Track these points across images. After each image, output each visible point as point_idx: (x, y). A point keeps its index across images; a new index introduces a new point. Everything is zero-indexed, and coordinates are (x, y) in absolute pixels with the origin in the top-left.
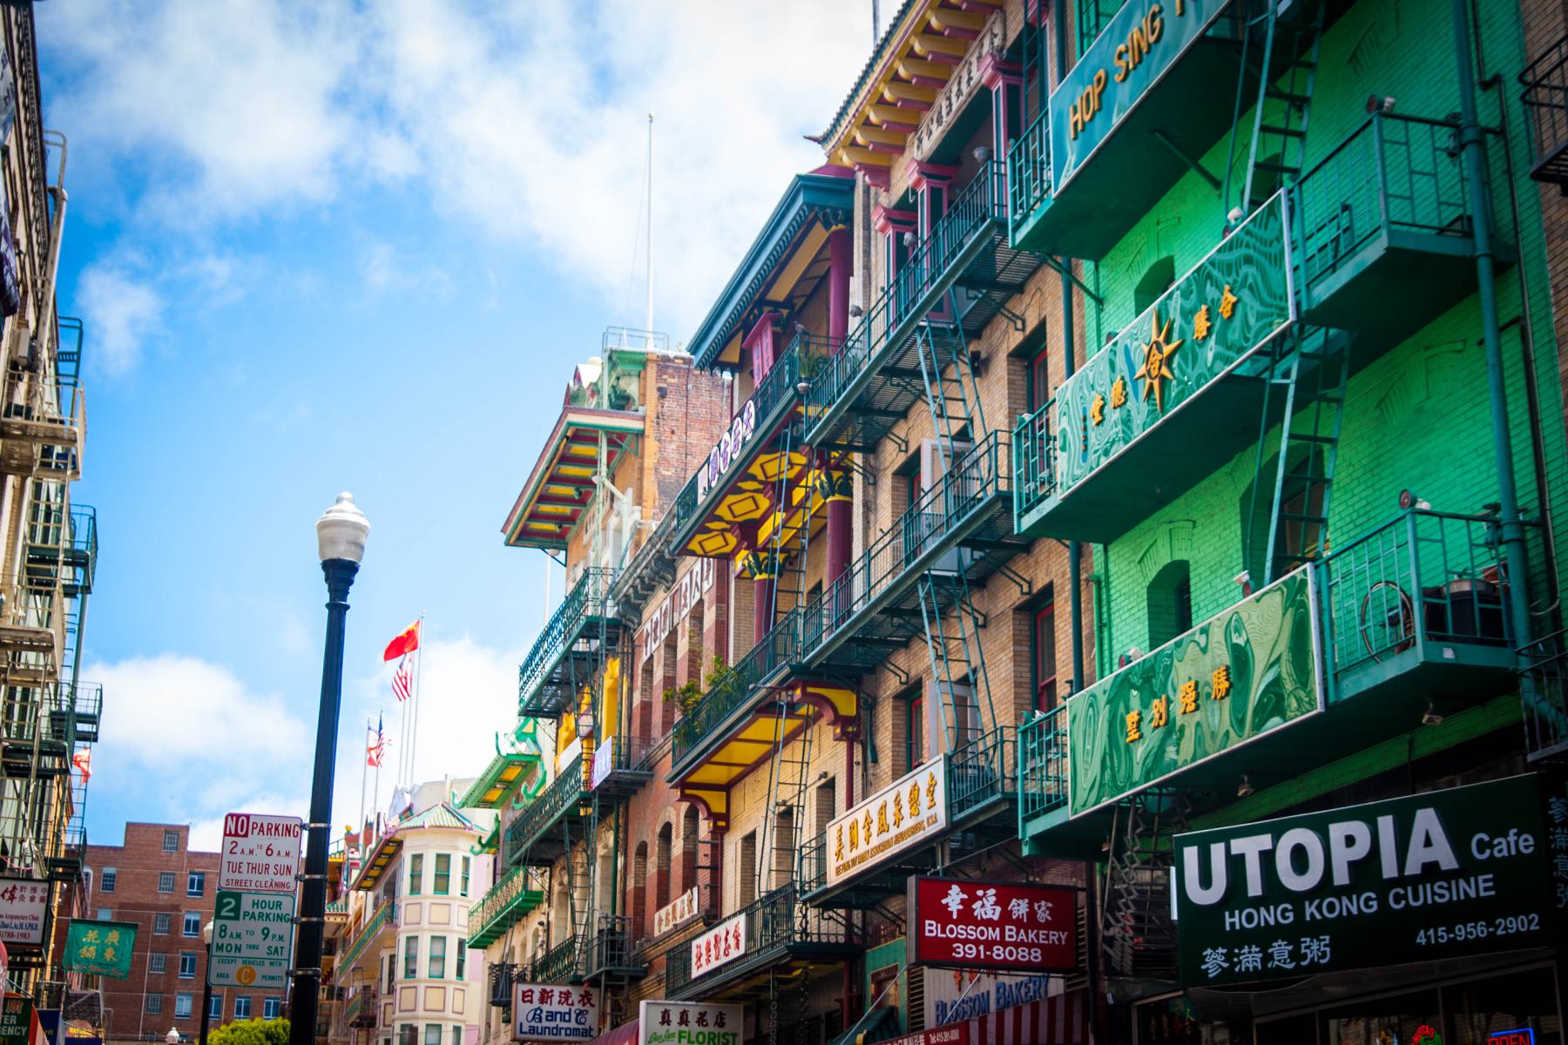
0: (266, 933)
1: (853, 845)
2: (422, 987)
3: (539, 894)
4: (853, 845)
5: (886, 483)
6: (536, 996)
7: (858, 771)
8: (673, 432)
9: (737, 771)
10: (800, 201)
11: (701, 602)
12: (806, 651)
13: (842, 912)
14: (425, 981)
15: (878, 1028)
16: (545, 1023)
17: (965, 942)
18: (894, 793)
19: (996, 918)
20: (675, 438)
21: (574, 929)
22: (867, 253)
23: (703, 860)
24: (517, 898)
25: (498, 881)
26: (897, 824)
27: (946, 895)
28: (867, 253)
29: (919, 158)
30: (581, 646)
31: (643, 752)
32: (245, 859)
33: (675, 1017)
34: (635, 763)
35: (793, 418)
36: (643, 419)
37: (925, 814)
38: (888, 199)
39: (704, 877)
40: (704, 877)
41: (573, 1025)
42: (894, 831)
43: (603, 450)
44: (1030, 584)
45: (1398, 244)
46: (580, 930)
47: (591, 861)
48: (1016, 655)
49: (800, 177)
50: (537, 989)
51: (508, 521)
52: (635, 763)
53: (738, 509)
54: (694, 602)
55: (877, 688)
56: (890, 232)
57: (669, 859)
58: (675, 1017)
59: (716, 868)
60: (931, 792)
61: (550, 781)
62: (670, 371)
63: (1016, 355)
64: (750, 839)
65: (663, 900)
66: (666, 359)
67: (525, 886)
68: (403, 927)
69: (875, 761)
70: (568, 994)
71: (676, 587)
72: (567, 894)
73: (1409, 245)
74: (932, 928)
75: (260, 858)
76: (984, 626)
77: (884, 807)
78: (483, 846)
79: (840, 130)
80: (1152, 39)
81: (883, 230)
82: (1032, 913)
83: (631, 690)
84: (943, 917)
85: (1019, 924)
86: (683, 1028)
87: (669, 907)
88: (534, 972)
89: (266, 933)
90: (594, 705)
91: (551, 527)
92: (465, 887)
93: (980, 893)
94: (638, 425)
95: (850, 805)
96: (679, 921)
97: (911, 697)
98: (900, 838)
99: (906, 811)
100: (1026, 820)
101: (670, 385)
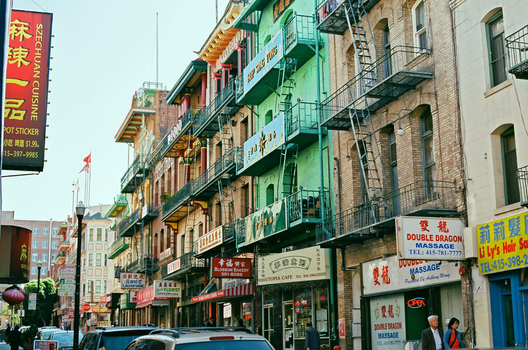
0: (69, 286)
1: (204, 244)
2: (94, 269)
3: (128, 245)
4: (204, 244)
5: (215, 147)
6: (127, 276)
7: (208, 222)
8: (164, 113)
9: (179, 218)
10: (193, 68)
11: (170, 168)
12: (194, 192)
13: (204, 259)
14: (95, 267)
15: (211, 289)
16: (130, 284)
17: (224, 272)
18: (215, 231)
19: (232, 266)
20: (164, 115)
21: (138, 257)
22: (210, 83)
23: (172, 241)
24: (122, 246)
25: (116, 240)
26: (213, 241)
27: (220, 261)
28: (210, 83)
29: (222, 62)
30: (138, 175)
31: (156, 207)
32: (65, 272)
33: (163, 285)
34: (154, 211)
35: (191, 128)
36: (155, 109)
37: (218, 239)
38: (215, 70)
39: (172, 245)
40: (172, 245)
41: (138, 284)
42: (212, 243)
43: (143, 117)
44: (244, 182)
45: (301, 132)
46: (139, 258)
47: (142, 238)
48: (242, 199)
49: (192, 61)
50: (127, 274)
51: (116, 135)
52: (154, 211)
53: (178, 147)
54: (169, 168)
55: (212, 201)
56: (216, 79)
57: (163, 238)
58: (163, 285)
59: (175, 243)
60: (220, 234)
61: (131, 214)
62: (163, 95)
63: (242, 122)
64: (183, 236)
65: (162, 250)
66: (161, 91)
67: (124, 242)
68: (88, 251)
69: (212, 220)
70: (136, 276)
71: (164, 162)
72: (136, 244)
73: (304, 132)
74: (216, 269)
75: (68, 272)
76: (235, 191)
77: (210, 236)
78: (111, 229)
79: (202, 52)
80: (262, 66)
81: (214, 78)
82: (240, 265)
83: (153, 189)
84: (219, 266)
85: (237, 267)
86: (165, 287)
87: (163, 252)
88: (127, 269)
89: (69, 286)
90: (143, 192)
91: (130, 137)
92: (106, 238)
93: (228, 260)
94: (154, 111)
95: (206, 233)
96: (166, 257)
97: (219, 204)
98: (214, 244)
99: (215, 238)
100: (238, 244)
101: (164, 99)
